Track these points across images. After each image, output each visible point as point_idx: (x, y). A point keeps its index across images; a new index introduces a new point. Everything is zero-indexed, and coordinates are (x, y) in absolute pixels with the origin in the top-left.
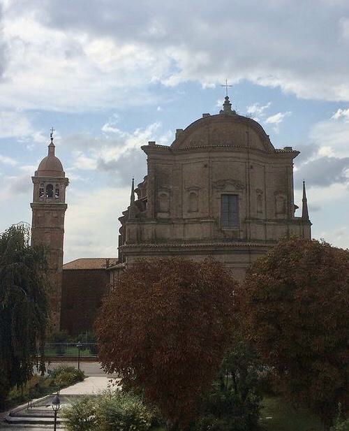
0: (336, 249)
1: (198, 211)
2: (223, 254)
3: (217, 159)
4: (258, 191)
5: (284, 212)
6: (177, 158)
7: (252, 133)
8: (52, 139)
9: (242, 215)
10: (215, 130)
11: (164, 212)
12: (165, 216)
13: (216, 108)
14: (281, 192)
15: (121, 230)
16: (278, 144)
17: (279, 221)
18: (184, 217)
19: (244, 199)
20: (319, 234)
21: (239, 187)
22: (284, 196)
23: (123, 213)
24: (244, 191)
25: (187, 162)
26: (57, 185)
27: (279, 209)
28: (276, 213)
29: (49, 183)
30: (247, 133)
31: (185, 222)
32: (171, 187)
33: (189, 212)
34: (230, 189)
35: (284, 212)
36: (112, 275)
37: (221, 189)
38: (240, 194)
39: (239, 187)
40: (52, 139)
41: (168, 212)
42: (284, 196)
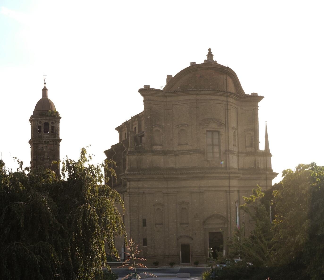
0: (277, 175)
1: (187, 144)
4: (233, 128)
5: (251, 146)
6: (169, 99)
7: (230, 81)
8: (45, 83)
10: (200, 77)
11: (158, 145)
12: (159, 148)
13: (201, 59)
15: (31, 148)
16: (248, 90)
18: (175, 150)
24: (224, 128)
26: (52, 123)
28: (246, 147)
29: (46, 121)
30: (226, 80)
31: (176, 154)
32: (163, 124)
33: (179, 145)
35: (251, 146)
40: (45, 83)
41: (161, 145)
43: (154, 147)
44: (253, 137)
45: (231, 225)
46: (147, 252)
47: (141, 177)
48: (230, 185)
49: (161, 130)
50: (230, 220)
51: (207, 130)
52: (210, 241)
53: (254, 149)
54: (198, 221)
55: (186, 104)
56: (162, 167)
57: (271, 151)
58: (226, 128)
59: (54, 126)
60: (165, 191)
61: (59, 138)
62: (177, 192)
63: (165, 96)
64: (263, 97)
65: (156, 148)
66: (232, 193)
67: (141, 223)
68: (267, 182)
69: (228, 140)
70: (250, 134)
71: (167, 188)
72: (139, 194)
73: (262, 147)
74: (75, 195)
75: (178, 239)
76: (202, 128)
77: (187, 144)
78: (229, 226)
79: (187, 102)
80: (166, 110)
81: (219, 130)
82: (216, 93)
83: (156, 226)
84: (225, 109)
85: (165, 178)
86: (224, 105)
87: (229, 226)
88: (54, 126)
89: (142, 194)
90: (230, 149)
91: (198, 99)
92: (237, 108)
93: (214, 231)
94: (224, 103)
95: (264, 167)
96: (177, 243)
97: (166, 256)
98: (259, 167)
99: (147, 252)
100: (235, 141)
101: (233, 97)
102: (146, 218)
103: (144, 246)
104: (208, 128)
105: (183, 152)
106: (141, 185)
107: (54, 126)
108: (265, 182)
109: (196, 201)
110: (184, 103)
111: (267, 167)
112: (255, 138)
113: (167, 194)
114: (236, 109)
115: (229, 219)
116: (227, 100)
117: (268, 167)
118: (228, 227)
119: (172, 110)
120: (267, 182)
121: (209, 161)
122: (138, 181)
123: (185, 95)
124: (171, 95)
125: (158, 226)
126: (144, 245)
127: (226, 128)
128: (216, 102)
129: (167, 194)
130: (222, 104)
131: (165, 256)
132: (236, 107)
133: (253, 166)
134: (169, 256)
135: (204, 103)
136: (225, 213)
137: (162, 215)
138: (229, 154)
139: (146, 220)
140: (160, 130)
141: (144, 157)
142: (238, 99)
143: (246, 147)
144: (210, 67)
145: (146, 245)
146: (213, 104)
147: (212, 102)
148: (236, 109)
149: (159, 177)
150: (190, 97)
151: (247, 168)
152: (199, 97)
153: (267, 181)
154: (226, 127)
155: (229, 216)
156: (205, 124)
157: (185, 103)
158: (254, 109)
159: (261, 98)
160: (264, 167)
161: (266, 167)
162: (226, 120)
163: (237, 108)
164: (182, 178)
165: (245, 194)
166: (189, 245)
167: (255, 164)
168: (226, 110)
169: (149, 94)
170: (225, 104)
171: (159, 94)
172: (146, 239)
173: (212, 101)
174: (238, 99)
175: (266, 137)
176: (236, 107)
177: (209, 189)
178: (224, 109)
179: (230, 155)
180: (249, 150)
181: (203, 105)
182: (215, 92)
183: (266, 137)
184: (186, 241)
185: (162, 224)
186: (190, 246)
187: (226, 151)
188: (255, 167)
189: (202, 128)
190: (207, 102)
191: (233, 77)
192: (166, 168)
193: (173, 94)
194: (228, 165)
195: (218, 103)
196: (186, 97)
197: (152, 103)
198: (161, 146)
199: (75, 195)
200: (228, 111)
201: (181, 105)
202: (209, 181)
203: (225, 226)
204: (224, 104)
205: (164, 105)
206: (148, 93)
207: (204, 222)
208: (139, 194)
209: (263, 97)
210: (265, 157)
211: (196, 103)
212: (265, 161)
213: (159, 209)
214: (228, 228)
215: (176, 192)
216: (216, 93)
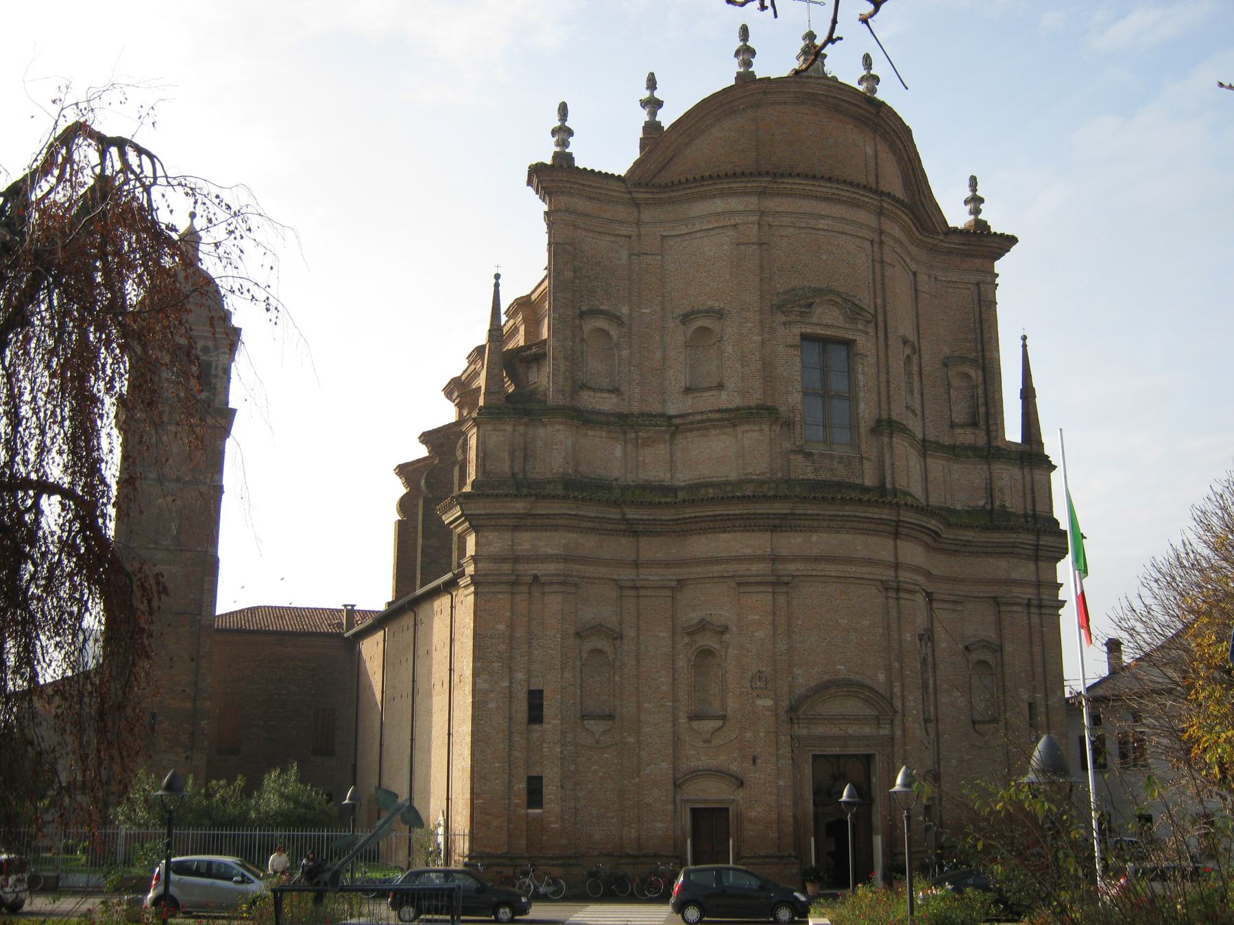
1: (721, 386)
2: (813, 530)
3: (787, 220)
9: (866, 411)
12: (606, 403)
14: (963, 360)
17: (955, 452)
18: (672, 411)
19: (872, 359)
20: (1055, 516)
21: (854, 312)
22: (972, 373)
23: (426, 438)
24: (871, 330)
25: (684, 230)
27: (959, 418)
28: (953, 426)
31: (674, 426)
32: (625, 310)
33: (688, 390)
34: (828, 320)
36: (881, 114)
37: (801, 314)
38: (861, 340)
39: (854, 312)
41: (615, 391)
42: (972, 373)
43: (586, 397)
44: (980, 391)
45: (904, 730)
46: (544, 838)
47: (526, 511)
48: (900, 560)
49: (614, 333)
50: (900, 705)
51: (804, 330)
52: (816, 793)
53: (983, 433)
54: (769, 702)
55: (717, 231)
56: (616, 479)
57: (1051, 448)
58: (877, 333)
59: (211, 362)
60: (626, 575)
61: (227, 403)
62: (679, 581)
63: (634, 199)
64: (1012, 240)
65: (592, 400)
66: (907, 596)
67: (521, 707)
68: (1037, 567)
69: (888, 382)
70: (968, 376)
71: (636, 564)
72: (513, 584)
73: (1013, 432)
74: (174, 515)
75: (677, 786)
76: (784, 324)
77: (723, 387)
78: (898, 733)
79: (721, 225)
80: (638, 255)
81: (851, 337)
82: (837, 192)
83: (586, 722)
84: (873, 260)
85: (629, 520)
86: (867, 245)
87: (898, 733)
88: (211, 362)
89: (531, 583)
90: (895, 418)
91: (768, 210)
92: (915, 274)
93: (836, 751)
94: (871, 235)
95: (1025, 508)
96: (675, 803)
97: (628, 855)
98: (1004, 506)
99: (544, 838)
100: (912, 393)
101: (900, 218)
102: (541, 688)
103: (530, 811)
104: (808, 324)
105: (705, 417)
106: (527, 546)
107: (211, 359)
108: (1032, 566)
109: (756, 617)
110: (711, 226)
111: (1037, 509)
112: (985, 390)
113: (636, 588)
114: (912, 278)
115: (898, 704)
116: (880, 226)
117: (1039, 508)
118: (892, 738)
119: (660, 257)
120: (1037, 567)
121: (811, 454)
122: (516, 528)
123: (715, 196)
124: (658, 196)
125: (592, 722)
126: (530, 806)
127: (877, 333)
128: (836, 229)
129: (636, 588)
130: (862, 238)
131: (620, 857)
132: (914, 267)
133: (981, 503)
134: (636, 857)
135: (792, 230)
136: (881, 677)
137: (614, 677)
138: (891, 436)
139: (542, 698)
140: (611, 333)
141: (541, 431)
142: (917, 234)
143: (953, 426)
144: (810, 91)
145: (540, 806)
146: (824, 236)
147: (820, 226)
148: (911, 274)
149: (601, 515)
150: (735, 203)
151: (959, 507)
152: (771, 204)
153: (1037, 564)
154: (876, 329)
155: (897, 690)
156: (796, 309)
157: (713, 229)
158: (978, 284)
159: (1008, 241)
160: (1025, 508)
161: (1034, 510)
162: (879, 301)
163: (915, 274)
164: (697, 522)
165: (954, 610)
166: (727, 810)
167: (990, 493)
168: (878, 266)
169: (568, 185)
170: (872, 242)
171: (608, 189)
172: (539, 779)
173: (822, 224)
174: (918, 239)
175: (1028, 394)
176: (914, 267)
177: (814, 570)
178: (870, 261)
179: (894, 439)
180: (966, 437)
181: (787, 236)
182: (834, 186)
183: (1028, 394)
184: (711, 792)
185: (610, 717)
186: (731, 813)
187: (879, 421)
188: (989, 507)
189: (784, 324)
190: (803, 225)
191: (901, 146)
192: (633, 481)
193: (664, 192)
194: (888, 478)
195: (846, 234)
196: (719, 205)
197: (582, 225)
198: (613, 396)
199: (174, 515)
200: (882, 269)
201: (699, 235)
202: (814, 538)
203: (882, 732)
204: (867, 240)
205: (630, 237)
206: (567, 181)
207: (793, 709)
208: (513, 584)
209: (1012, 240)
210: (1026, 470)
211: (759, 224)
212: (1028, 486)
213: (599, 652)
214: (892, 739)
215: (673, 584)
216: (837, 192)
